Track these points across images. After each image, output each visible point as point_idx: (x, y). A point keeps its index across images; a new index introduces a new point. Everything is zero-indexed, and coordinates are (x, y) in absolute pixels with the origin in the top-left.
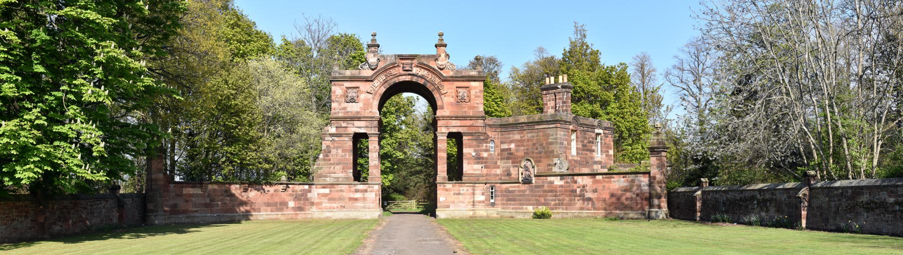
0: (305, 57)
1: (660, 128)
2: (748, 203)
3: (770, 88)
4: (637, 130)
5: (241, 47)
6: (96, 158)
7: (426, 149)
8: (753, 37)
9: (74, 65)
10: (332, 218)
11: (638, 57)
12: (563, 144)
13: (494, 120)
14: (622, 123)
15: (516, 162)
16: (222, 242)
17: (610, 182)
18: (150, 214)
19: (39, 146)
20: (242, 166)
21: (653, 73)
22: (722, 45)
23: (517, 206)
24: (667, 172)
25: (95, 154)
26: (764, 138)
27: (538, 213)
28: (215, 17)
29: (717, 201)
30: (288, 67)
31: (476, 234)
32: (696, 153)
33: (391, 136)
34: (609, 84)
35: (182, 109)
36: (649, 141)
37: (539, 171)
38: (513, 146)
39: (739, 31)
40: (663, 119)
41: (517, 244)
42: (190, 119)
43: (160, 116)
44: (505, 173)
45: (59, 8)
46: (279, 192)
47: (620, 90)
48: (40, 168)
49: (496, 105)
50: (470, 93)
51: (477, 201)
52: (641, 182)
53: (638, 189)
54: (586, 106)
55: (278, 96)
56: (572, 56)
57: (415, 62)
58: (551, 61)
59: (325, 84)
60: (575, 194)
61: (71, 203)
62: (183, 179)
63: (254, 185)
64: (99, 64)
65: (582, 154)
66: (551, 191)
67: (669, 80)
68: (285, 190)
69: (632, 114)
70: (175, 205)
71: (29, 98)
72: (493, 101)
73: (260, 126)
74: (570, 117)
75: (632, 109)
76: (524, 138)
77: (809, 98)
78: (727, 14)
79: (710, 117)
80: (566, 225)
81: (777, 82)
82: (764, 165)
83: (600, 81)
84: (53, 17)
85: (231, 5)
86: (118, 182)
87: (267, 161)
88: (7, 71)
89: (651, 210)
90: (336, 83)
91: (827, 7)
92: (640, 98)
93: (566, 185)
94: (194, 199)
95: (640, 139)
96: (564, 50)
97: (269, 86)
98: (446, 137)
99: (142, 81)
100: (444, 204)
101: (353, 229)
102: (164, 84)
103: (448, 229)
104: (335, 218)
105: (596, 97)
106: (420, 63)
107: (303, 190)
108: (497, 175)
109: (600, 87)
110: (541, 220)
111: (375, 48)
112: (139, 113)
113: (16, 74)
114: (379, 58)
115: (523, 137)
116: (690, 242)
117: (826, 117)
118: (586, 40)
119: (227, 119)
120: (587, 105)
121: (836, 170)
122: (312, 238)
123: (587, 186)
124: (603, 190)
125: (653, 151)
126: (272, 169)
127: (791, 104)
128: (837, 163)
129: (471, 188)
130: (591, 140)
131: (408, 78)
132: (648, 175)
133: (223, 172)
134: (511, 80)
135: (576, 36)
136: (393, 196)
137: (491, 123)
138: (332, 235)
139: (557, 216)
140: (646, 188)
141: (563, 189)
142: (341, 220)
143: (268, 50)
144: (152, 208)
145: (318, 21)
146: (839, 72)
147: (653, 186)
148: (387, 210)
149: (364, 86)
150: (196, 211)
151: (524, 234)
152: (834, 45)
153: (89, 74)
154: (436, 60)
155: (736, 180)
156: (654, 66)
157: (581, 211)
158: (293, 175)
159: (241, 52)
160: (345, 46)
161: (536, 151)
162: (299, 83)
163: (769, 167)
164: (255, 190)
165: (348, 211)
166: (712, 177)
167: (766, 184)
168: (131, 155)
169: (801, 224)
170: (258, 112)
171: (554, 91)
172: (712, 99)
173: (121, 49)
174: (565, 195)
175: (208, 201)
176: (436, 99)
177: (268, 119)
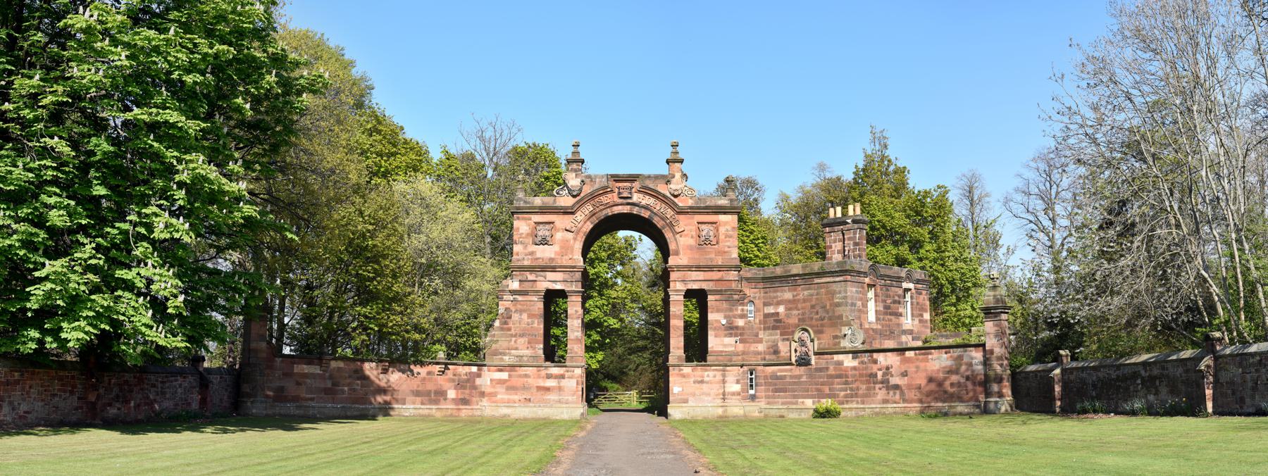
2: (1129, 382)
3: (1153, 218)
6: (172, 317)
7: (652, 314)
8: (1128, 146)
9: (146, 187)
10: (512, 417)
13: (754, 271)
14: (941, 272)
15: (787, 333)
17: (927, 360)
18: (245, 400)
19: (93, 297)
20: (382, 336)
21: (987, 199)
22: (1085, 158)
23: (788, 400)
25: (170, 311)
26: (1147, 290)
27: (821, 410)
29: (1083, 382)
30: (450, 192)
31: (727, 443)
32: (1050, 313)
33: (601, 295)
37: (821, 346)
38: (781, 309)
39: (1108, 138)
41: (790, 459)
42: (308, 264)
44: (772, 350)
45: (127, 109)
47: (937, 225)
48: (95, 327)
49: (756, 249)
50: (718, 230)
51: (729, 393)
52: (972, 358)
54: (889, 248)
55: (435, 234)
56: (867, 176)
57: (637, 185)
58: (836, 183)
59: (504, 217)
61: (135, 377)
62: (295, 351)
63: (398, 365)
64: (181, 185)
65: (883, 319)
66: (839, 376)
68: (443, 372)
69: (956, 260)
70: (281, 389)
71: (83, 229)
72: (752, 243)
74: (865, 265)
77: (1209, 231)
78: (1090, 114)
79: (1069, 261)
80: (863, 426)
81: (1163, 210)
82: (1148, 328)
83: (908, 212)
84: (119, 122)
87: (417, 328)
88: (55, 194)
91: (1232, 104)
92: (967, 236)
93: (861, 366)
94: (308, 381)
98: (682, 297)
99: (240, 210)
101: (542, 434)
105: (903, 235)
108: (759, 353)
109: (908, 220)
110: (826, 419)
112: (235, 256)
113: (69, 197)
116: (1048, 446)
117: (1232, 256)
118: (887, 153)
120: (890, 248)
121: (1250, 330)
123: (892, 367)
124: (917, 372)
125: (989, 312)
126: (424, 340)
127: (1183, 240)
128: (1251, 320)
129: (721, 373)
130: (897, 298)
131: (626, 209)
132: (981, 348)
133: (353, 343)
134: (778, 211)
135: (873, 147)
137: (749, 275)
138: (510, 443)
139: (849, 414)
142: (525, 419)
143: (422, 167)
144: (248, 390)
146: (1248, 193)
147: (990, 365)
148: (595, 406)
149: (561, 221)
150: (312, 399)
152: (1241, 158)
153: (166, 199)
154: (668, 182)
155: (1110, 351)
156: (988, 189)
157: (884, 406)
158: (455, 351)
159: (382, 169)
162: (467, 215)
163: (1156, 329)
164: (399, 371)
165: (535, 406)
166: (1075, 348)
167: (1153, 355)
169: (1206, 409)
172: (1071, 235)
175: (329, 384)
177: (420, 268)
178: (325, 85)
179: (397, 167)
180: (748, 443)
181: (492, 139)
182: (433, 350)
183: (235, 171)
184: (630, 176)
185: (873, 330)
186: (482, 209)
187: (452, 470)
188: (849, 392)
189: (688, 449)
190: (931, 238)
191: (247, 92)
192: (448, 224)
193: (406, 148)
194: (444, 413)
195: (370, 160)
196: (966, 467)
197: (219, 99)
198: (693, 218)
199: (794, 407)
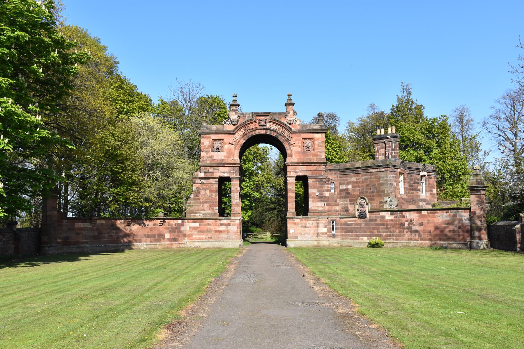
0: (178, 115)
1: (479, 169)
4: (458, 172)
5: (125, 106)
11: (457, 109)
12: (392, 185)
14: (443, 166)
15: (353, 200)
16: (107, 268)
17: (435, 217)
20: (127, 205)
21: (472, 122)
24: (486, 208)
27: (372, 243)
28: (102, 80)
30: (164, 123)
31: (320, 260)
33: (250, 179)
34: (432, 133)
35: (74, 157)
36: (468, 181)
38: (350, 187)
40: (481, 162)
41: (356, 269)
43: (55, 162)
46: (157, 225)
47: (441, 138)
50: (314, 143)
51: (320, 233)
52: (462, 216)
53: (459, 223)
54: (412, 152)
56: (399, 111)
57: (269, 118)
58: (381, 115)
59: (195, 137)
60: (404, 227)
63: (137, 221)
65: (409, 193)
66: (383, 224)
67: (486, 128)
68: (162, 224)
69: (452, 159)
70: (67, 238)
72: (333, 150)
73: (141, 172)
74: (398, 162)
75: (452, 154)
76: (359, 180)
80: (397, 253)
83: (424, 131)
85: (115, 71)
86: (16, 218)
87: (147, 200)
89: (472, 241)
90: (204, 136)
92: (459, 145)
93: (396, 219)
94: (84, 232)
95: (460, 179)
96: (393, 106)
97: (149, 138)
98: (294, 180)
99: (39, 133)
100: (293, 235)
102: (58, 136)
103: (298, 257)
104: (203, 247)
105: (420, 144)
106: (272, 119)
107: (177, 224)
108: (337, 211)
109: (423, 136)
110: (375, 248)
111: (236, 107)
112: (36, 160)
114: (239, 115)
115: (358, 179)
119: (113, 166)
122: (184, 264)
123: (414, 220)
124: (428, 223)
125: (473, 189)
126: (151, 207)
129: (316, 222)
130: (417, 181)
131: (263, 132)
132: (468, 211)
133: (110, 210)
134: (347, 132)
136: (252, 228)
137: (331, 168)
138: (201, 261)
139: (389, 246)
140: (467, 222)
141: (393, 222)
142: (209, 248)
143: (148, 109)
145: (188, 84)
148: (247, 241)
149: (227, 139)
150: (86, 243)
151: (361, 261)
154: (286, 116)
156: (472, 117)
157: (409, 242)
158: (169, 212)
159: (125, 110)
160: (211, 106)
161: (370, 191)
162: (174, 136)
164: (137, 224)
165: (214, 241)
168: (28, 195)
170: (139, 160)
171: (384, 140)
173: (18, 105)
174: (395, 227)
175: (96, 233)
176: (286, 149)
177: (148, 166)
178: (89, 58)
179: (133, 109)
180: (332, 260)
181: (188, 93)
182: (156, 211)
183: (34, 110)
184: (265, 113)
185: (402, 198)
186: (182, 132)
187: (169, 277)
188: (388, 233)
189: (299, 263)
190: (437, 146)
191: (39, 62)
192: (163, 141)
193: (139, 98)
194: (163, 247)
195: (118, 105)
196: (460, 279)
197: (20, 65)
198: (300, 136)
199: (357, 241)
